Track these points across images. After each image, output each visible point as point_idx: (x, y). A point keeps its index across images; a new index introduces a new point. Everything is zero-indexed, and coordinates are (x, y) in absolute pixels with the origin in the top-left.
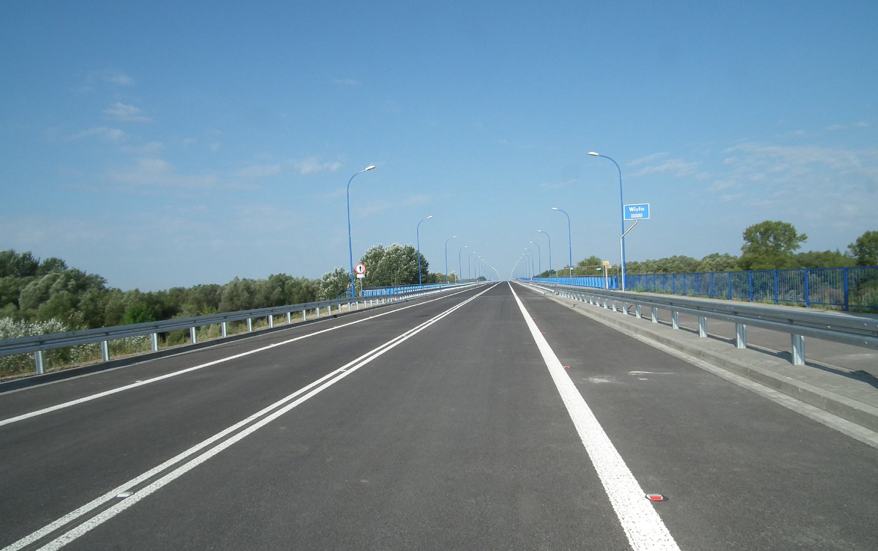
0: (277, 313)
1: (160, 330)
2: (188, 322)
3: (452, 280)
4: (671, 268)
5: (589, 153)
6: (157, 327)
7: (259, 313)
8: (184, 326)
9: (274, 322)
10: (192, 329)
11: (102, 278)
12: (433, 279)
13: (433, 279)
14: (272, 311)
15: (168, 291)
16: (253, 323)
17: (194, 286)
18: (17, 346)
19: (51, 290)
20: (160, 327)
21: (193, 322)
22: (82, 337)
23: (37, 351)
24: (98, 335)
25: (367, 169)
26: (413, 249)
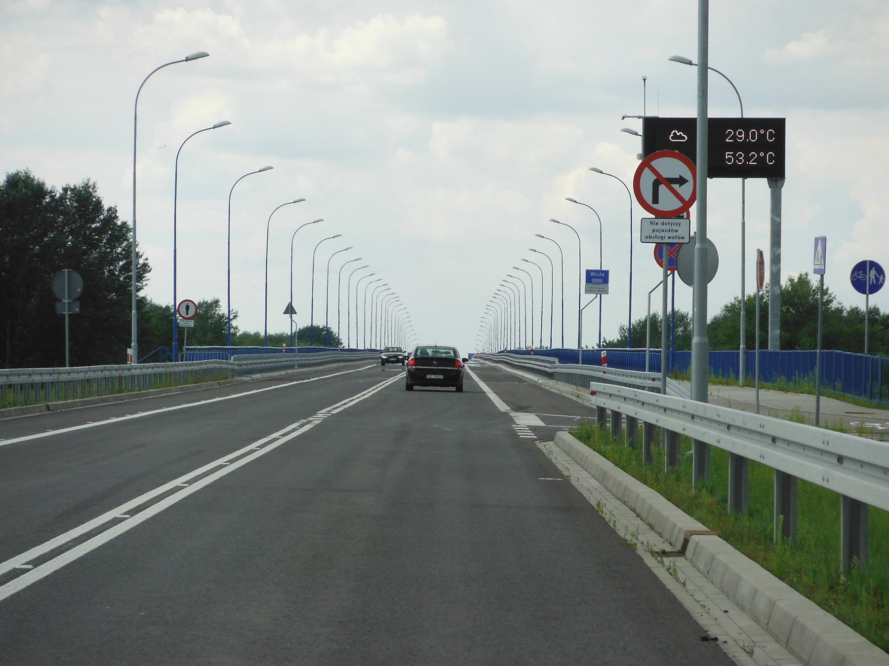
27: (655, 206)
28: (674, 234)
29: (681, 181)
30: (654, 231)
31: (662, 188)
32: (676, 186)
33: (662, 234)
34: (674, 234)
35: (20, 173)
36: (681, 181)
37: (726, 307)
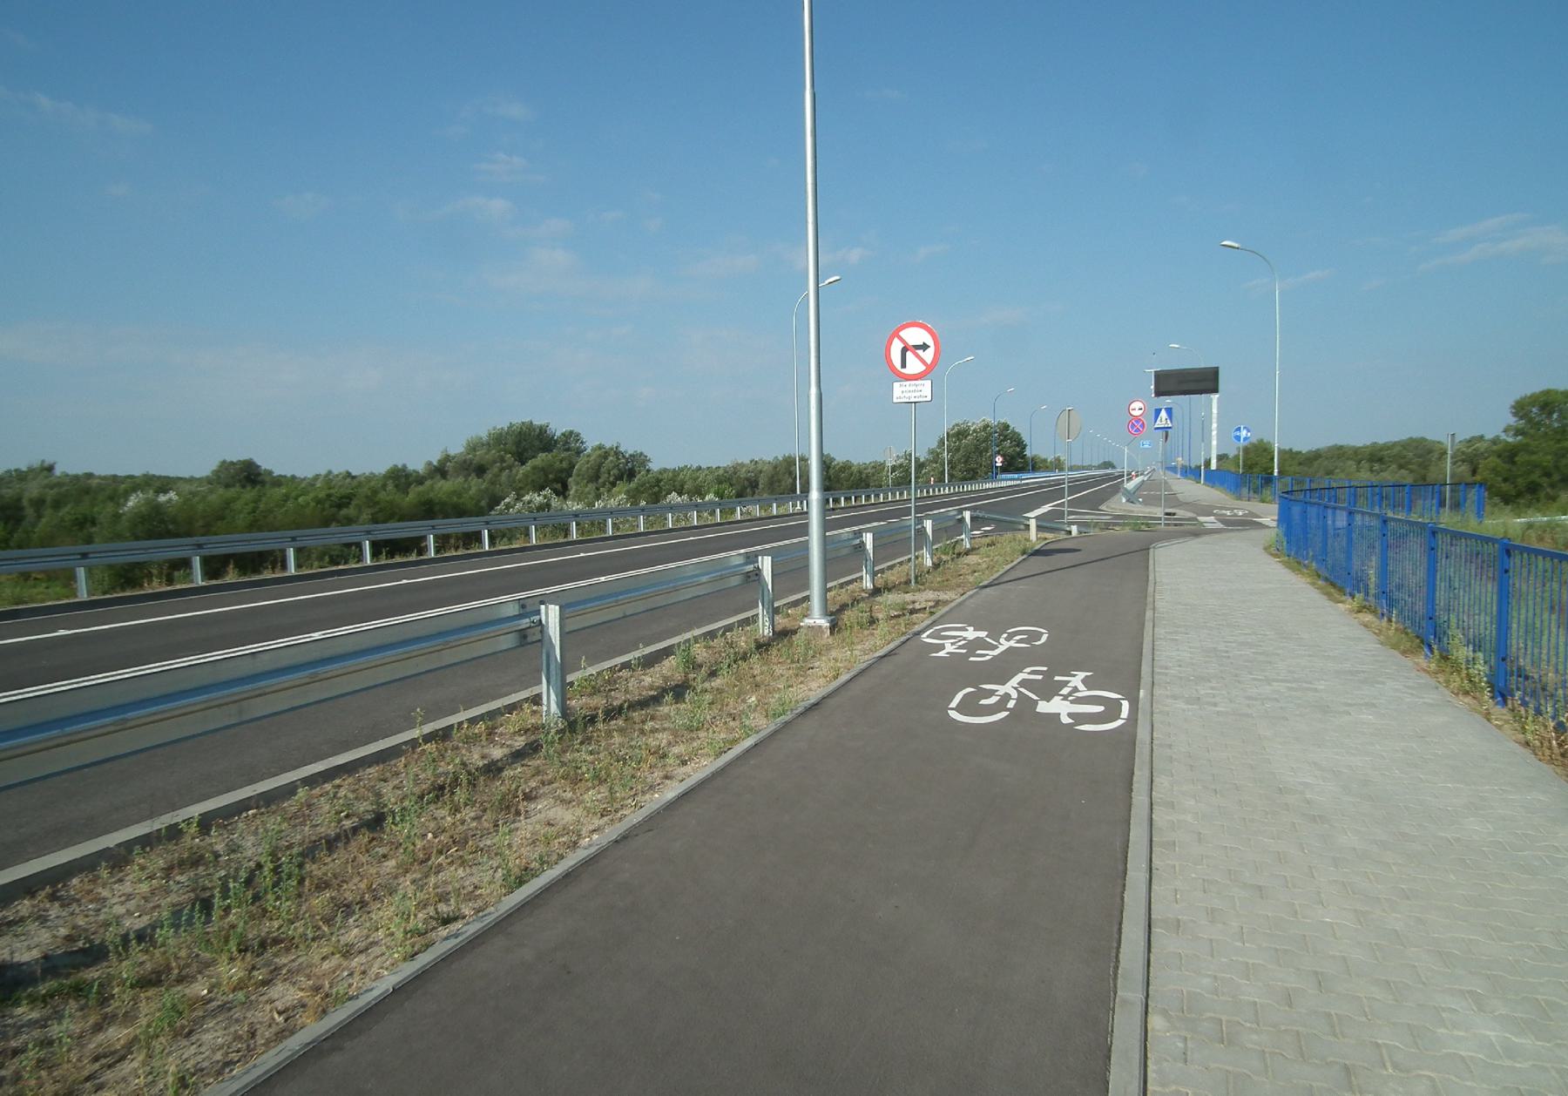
1: (299, 544)
2: (11, 559)
3: (1058, 465)
4: (1389, 457)
8: (4, 567)
11: (646, 457)
12: (1035, 465)
13: (1035, 465)
16: (492, 538)
18: (161, 550)
19: (602, 470)
20: (91, 555)
25: (827, 282)
26: (1008, 426)
27: (903, 371)
28: (918, 394)
29: (925, 347)
30: (903, 392)
31: (909, 355)
32: (920, 352)
33: (910, 394)
34: (918, 394)
35: (451, 914)
36: (925, 347)
37: (1262, 440)
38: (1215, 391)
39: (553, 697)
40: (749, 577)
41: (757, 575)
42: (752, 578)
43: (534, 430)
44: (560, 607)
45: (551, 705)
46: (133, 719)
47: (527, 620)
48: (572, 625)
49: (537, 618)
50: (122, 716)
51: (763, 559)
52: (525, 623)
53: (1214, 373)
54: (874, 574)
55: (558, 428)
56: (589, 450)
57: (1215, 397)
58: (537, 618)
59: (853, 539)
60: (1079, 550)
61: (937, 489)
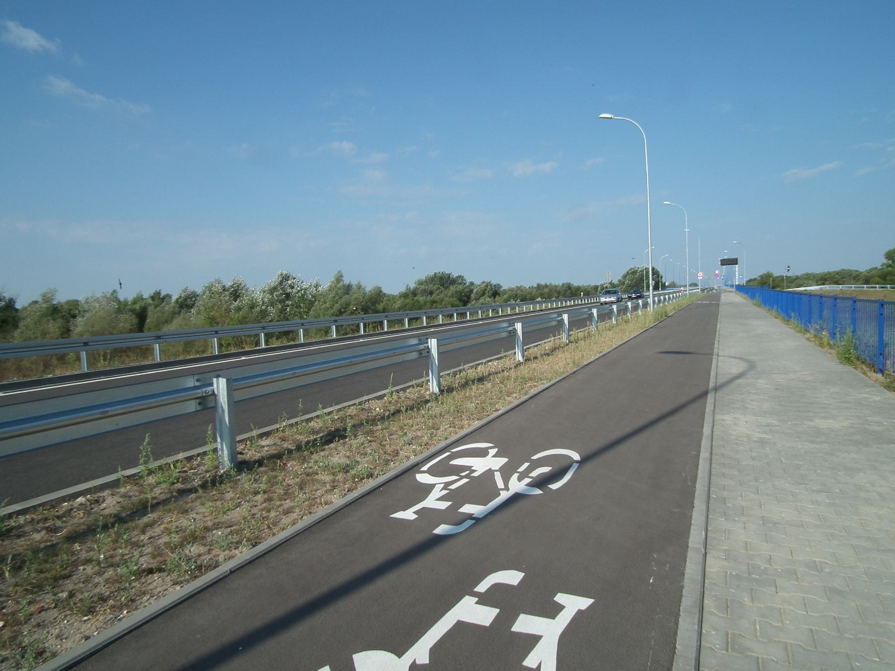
0: (460, 312)
5: (665, 203)
6: (336, 321)
7: (414, 313)
9: (305, 338)
10: (261, 334)
11: (484, 282)
14: (456, 310)
15: (503, 289)
17: (546, 284)
18: (226, 332)
21: (301, 325)
22: (137, 340)
23: (214, 338)
24: (182, 336)
26: (654, 268)
38: (737, 264)
39: (520, 353)
40: (510, 333)
41: (428, 352)
42: (512, 334)
43: (445, 277)
44: (227, 380)
45: (225, 454)
46: (297, 373)
47: (423, 346)
48: (239, 395)
49: (427, 345)
50: (294, 372)
51: (431, 340)
52: (422, 347)
53: (737, 259)
54: (524, 351)
55: (455, 274)
56: (467, 284)
57: (737, 266)
58: (427, 345)
59: (508, 327)
60: (440, 491)
61: (586, 300)
